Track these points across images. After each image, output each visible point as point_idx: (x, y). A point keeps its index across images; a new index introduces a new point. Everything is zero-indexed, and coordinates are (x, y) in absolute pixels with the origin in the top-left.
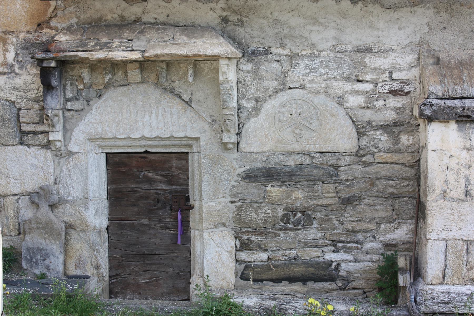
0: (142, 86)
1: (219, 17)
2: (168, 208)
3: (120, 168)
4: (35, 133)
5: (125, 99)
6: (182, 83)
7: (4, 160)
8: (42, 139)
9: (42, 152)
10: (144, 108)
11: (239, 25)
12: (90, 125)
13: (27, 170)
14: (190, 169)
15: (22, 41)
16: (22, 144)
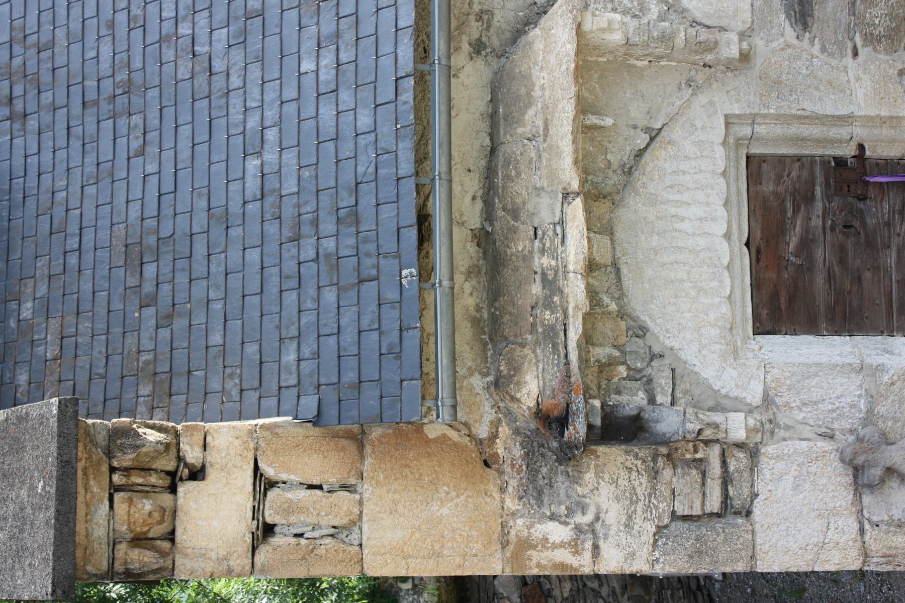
0: (619, 234)
1: (472, 59)
2: (861, 205)
3: (783, 306)
4: (726, 480)
5: (649, 272)
6: (610, 146)
7: (786, 552)
8: (738, 461)
9: (765, 464)
10: (665, 231)
11: (488, 20)
12: (704, 352)
13: (807, 501)
14: (783, 150)
15: (524, 505)
16: (749, 513)
